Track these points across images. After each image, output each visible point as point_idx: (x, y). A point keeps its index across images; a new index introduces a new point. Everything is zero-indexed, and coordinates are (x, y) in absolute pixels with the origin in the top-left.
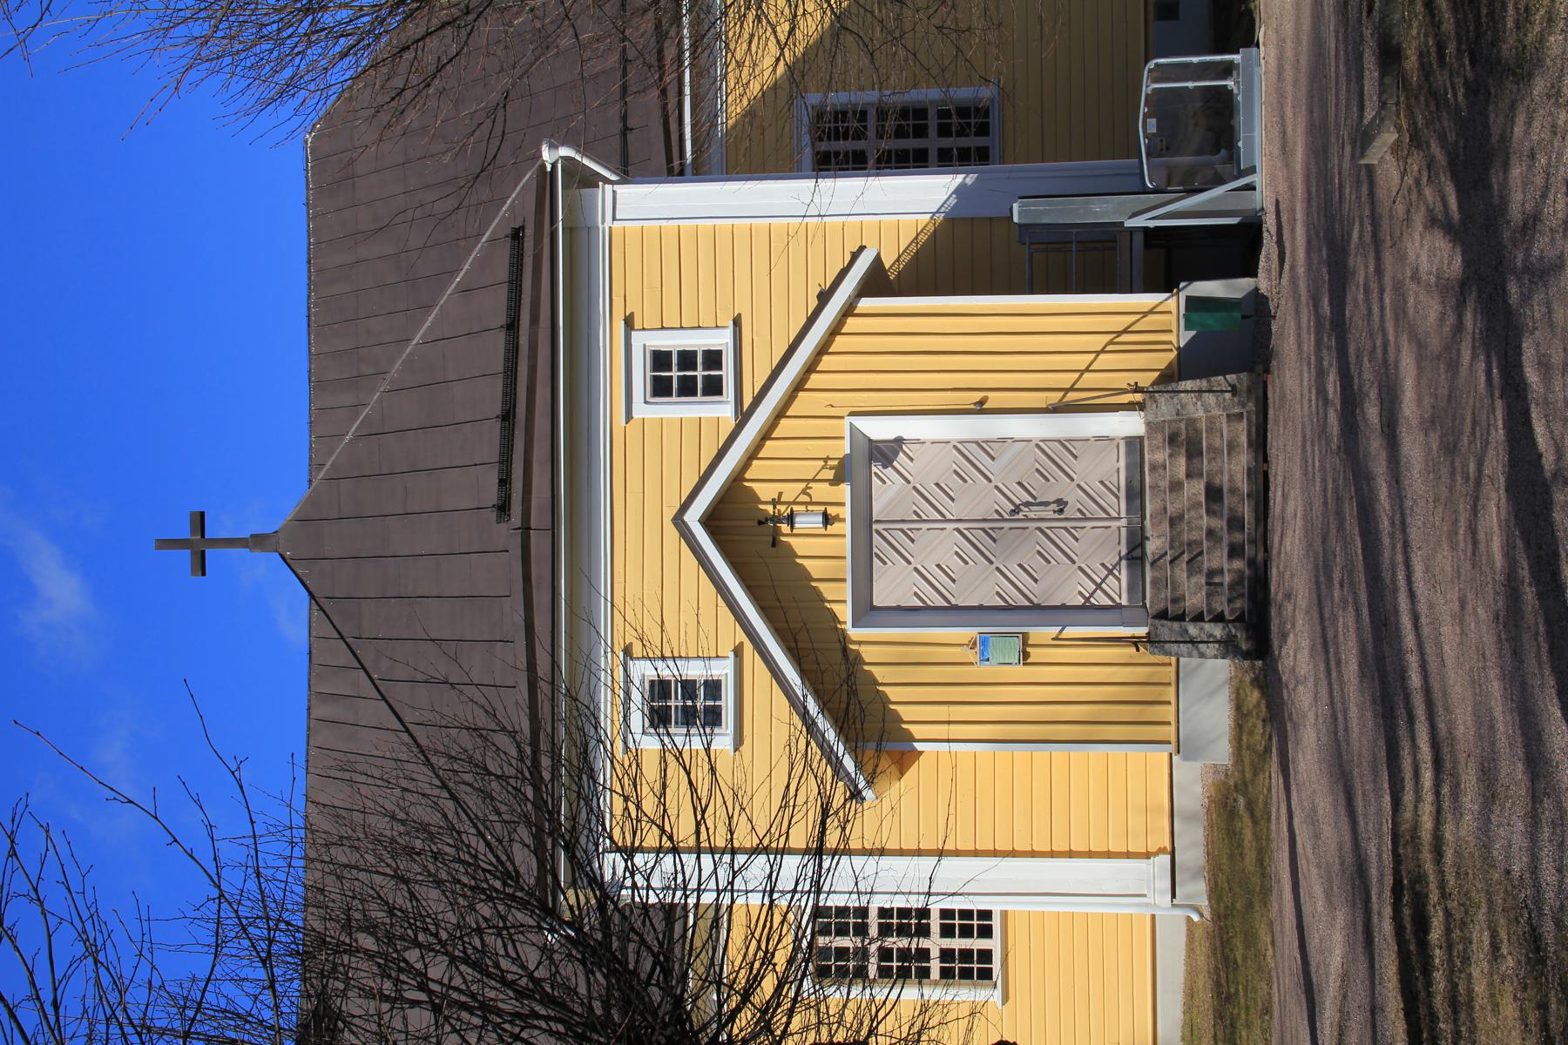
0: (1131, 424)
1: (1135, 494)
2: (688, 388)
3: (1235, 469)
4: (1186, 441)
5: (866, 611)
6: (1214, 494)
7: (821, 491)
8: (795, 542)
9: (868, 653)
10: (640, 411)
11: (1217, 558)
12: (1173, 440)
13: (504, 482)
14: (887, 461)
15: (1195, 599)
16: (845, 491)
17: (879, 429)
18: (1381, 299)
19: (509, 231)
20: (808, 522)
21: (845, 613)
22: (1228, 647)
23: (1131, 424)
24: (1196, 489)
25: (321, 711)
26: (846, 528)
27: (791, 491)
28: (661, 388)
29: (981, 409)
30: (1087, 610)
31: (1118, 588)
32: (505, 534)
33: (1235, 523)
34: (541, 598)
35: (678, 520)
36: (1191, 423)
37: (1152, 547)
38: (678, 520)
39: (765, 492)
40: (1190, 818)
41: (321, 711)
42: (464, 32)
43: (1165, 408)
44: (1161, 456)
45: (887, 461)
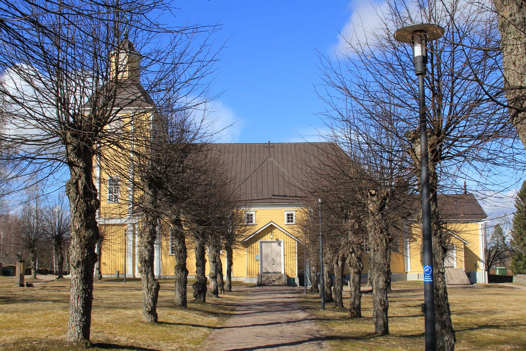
0: (283, 272)
1: (274, 273)
2: (288, 218)
3: (277, 283)
4: (280, 278)
5: (261, 243)
6: (274, 281)
7: (275, 237)
8: (269, 234)
9: (257, 243)
10: (286, 212)
11: (267, 281)
12: (280, 277)
13: (277, 196)
14: (278, 245)
15: (263, 279)
16: (275, 240)
17: (282, 244)
18: (51, 147)
19: (418, 8)
20: (271, 236)
21: (261, 240)
22: (258, 282)
23: (283, 272)
24: (274, 279)
25: (244, 146)
26: (271, 240)
27: (275, 234)
28: (288, 215)
29: (284, 255)
30: (262, 267)
31: (264, 271)
32: (270, 196)
33: (271, 283)
34: (262, 201)
35: (272, 222)
36: (282, 279)
37: (269, 274)
38: (272, 222)
39: (275, 231)
40: (237, 279)
41: (244, 146)
42: (406, 99)
43: (284, 276)
44: (279, 276)
45: (278, 245)
